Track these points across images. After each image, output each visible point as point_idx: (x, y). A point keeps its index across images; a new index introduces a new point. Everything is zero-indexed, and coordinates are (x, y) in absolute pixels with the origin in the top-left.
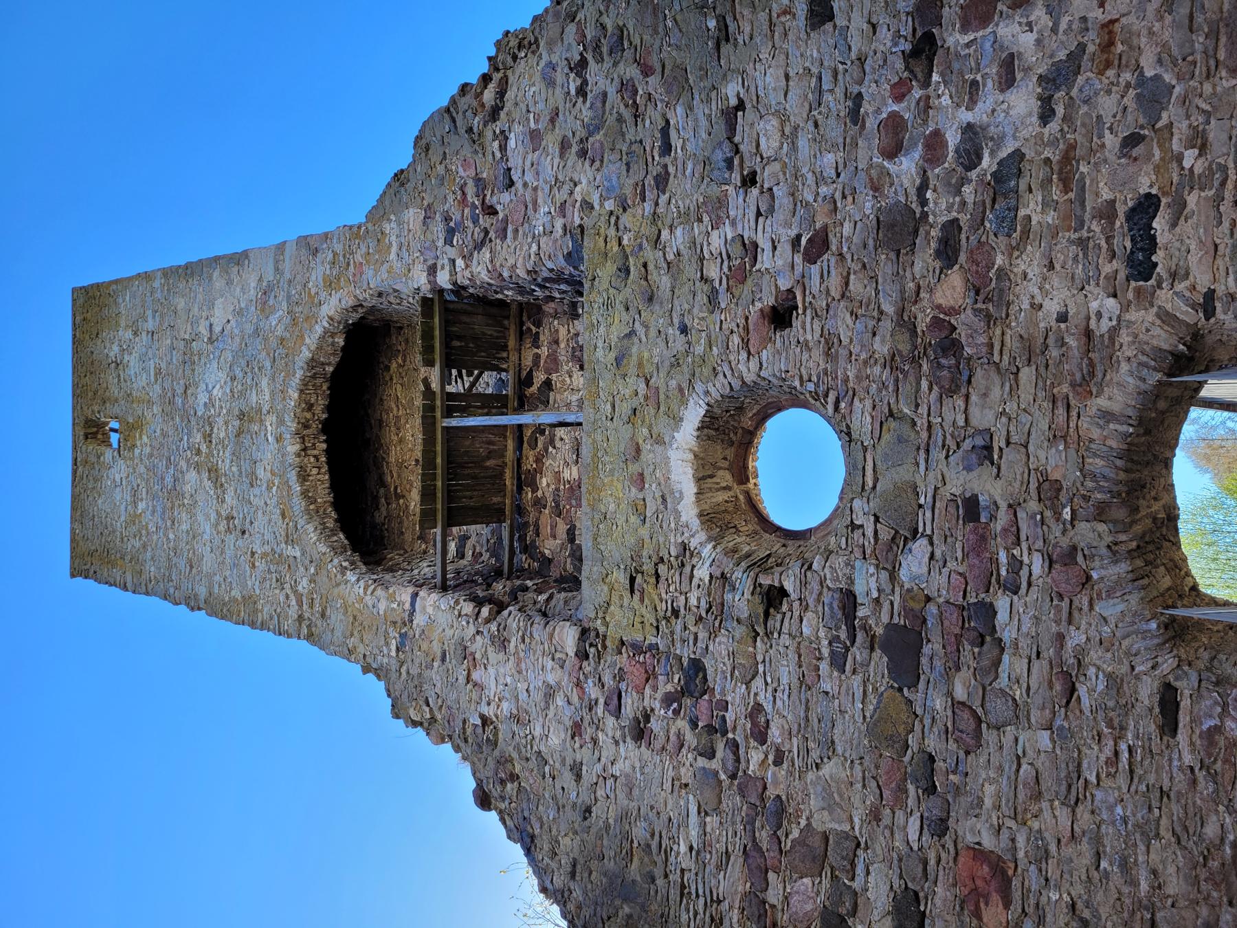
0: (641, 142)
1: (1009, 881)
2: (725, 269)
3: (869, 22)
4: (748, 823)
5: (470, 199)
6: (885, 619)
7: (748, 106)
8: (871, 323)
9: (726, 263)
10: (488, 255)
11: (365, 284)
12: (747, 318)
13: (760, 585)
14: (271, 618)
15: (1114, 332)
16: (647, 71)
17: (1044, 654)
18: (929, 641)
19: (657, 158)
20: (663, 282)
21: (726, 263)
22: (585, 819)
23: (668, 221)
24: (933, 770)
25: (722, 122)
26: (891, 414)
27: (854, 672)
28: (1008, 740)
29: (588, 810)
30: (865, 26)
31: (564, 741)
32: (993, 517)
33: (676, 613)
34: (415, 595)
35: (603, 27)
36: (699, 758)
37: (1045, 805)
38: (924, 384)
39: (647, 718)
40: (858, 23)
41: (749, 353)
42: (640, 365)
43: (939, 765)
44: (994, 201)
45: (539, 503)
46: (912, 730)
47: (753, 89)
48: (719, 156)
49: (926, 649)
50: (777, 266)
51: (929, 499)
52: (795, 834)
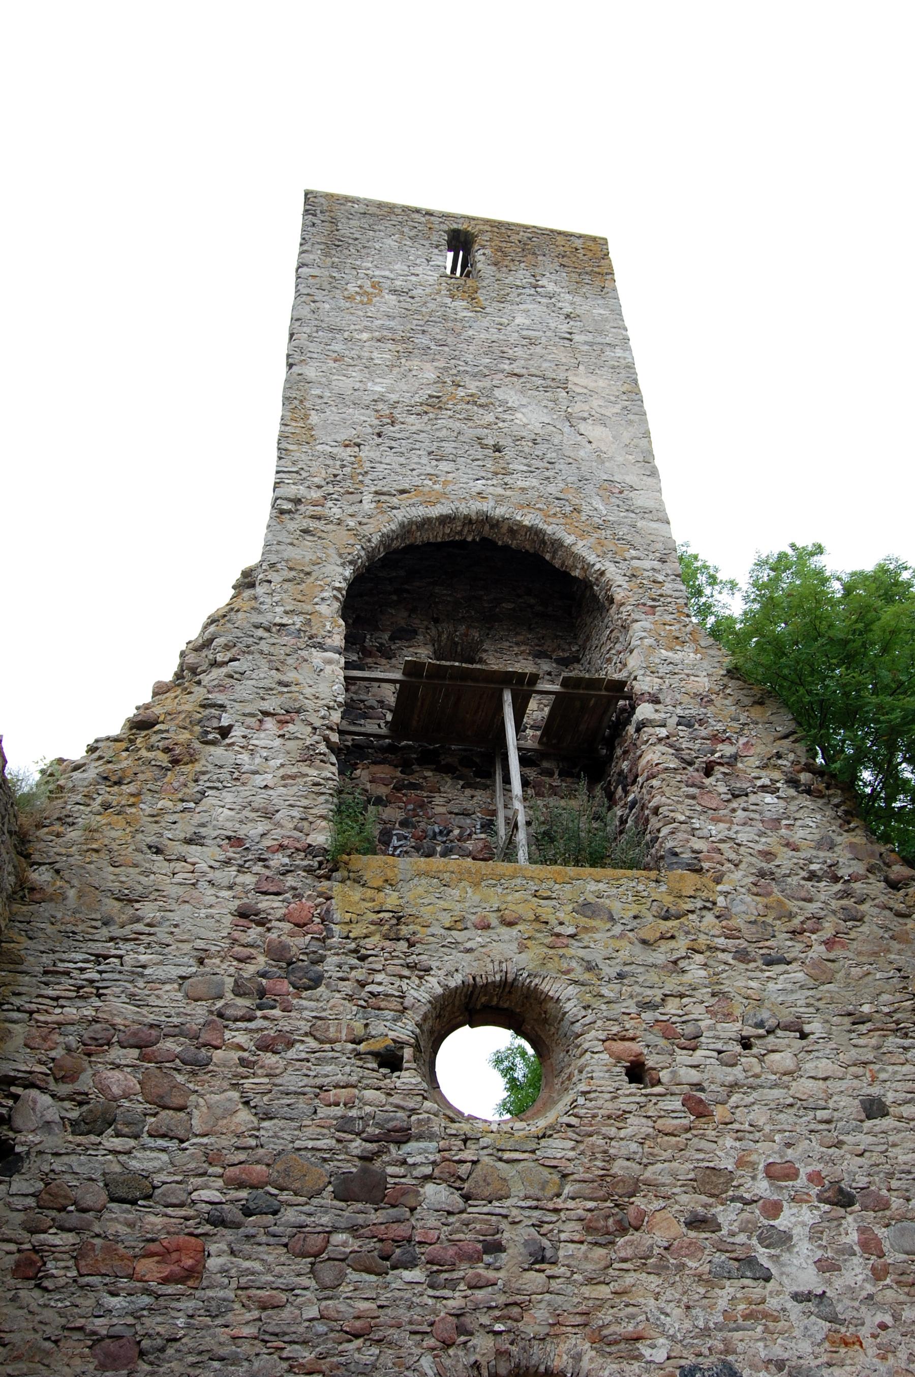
0: (774, 936)
1: (183, 1283)
2: (674, 1019)
3: (865, 1151)
4: (181, 1030)
5: (720, 747)
6: (390, 1170)
7: (804, 1042)
8: (637, 1157)
9: (679, 1019)
10: (672, 766)
11: (637, 617)
12: (633, 1039)
13: (402, 1048)
14: (294, 463)
15: (638, 1357)
16: (829, 944)
17: (381, 1312)
18: (376, 1210)
19: (762, 952)
20: (660, 956)
21: (679, 1019)
22: (150, 847)
23: (711, 962)
24: (266, 1214)
25: (790, 1018)
26: (565, 1176)
27: (339, 1141)
28: (305, 1281)
29: (159, 851)
30: (862, 1147)
32: (488, 1266)
33: (363, 958)
35: (862, 902)
36: (232, 979)
37: (256, 1314)
38: (591, 1204)
39: (261, 924)
40: (866, 1140)
41: (604, 1041)
42: (586, 929)
44: (736, 1259)
46: (296, 1194)
47: (816, 1048)
48: (765, 1015)
50: (680, 1068)
51: (498, 1211)
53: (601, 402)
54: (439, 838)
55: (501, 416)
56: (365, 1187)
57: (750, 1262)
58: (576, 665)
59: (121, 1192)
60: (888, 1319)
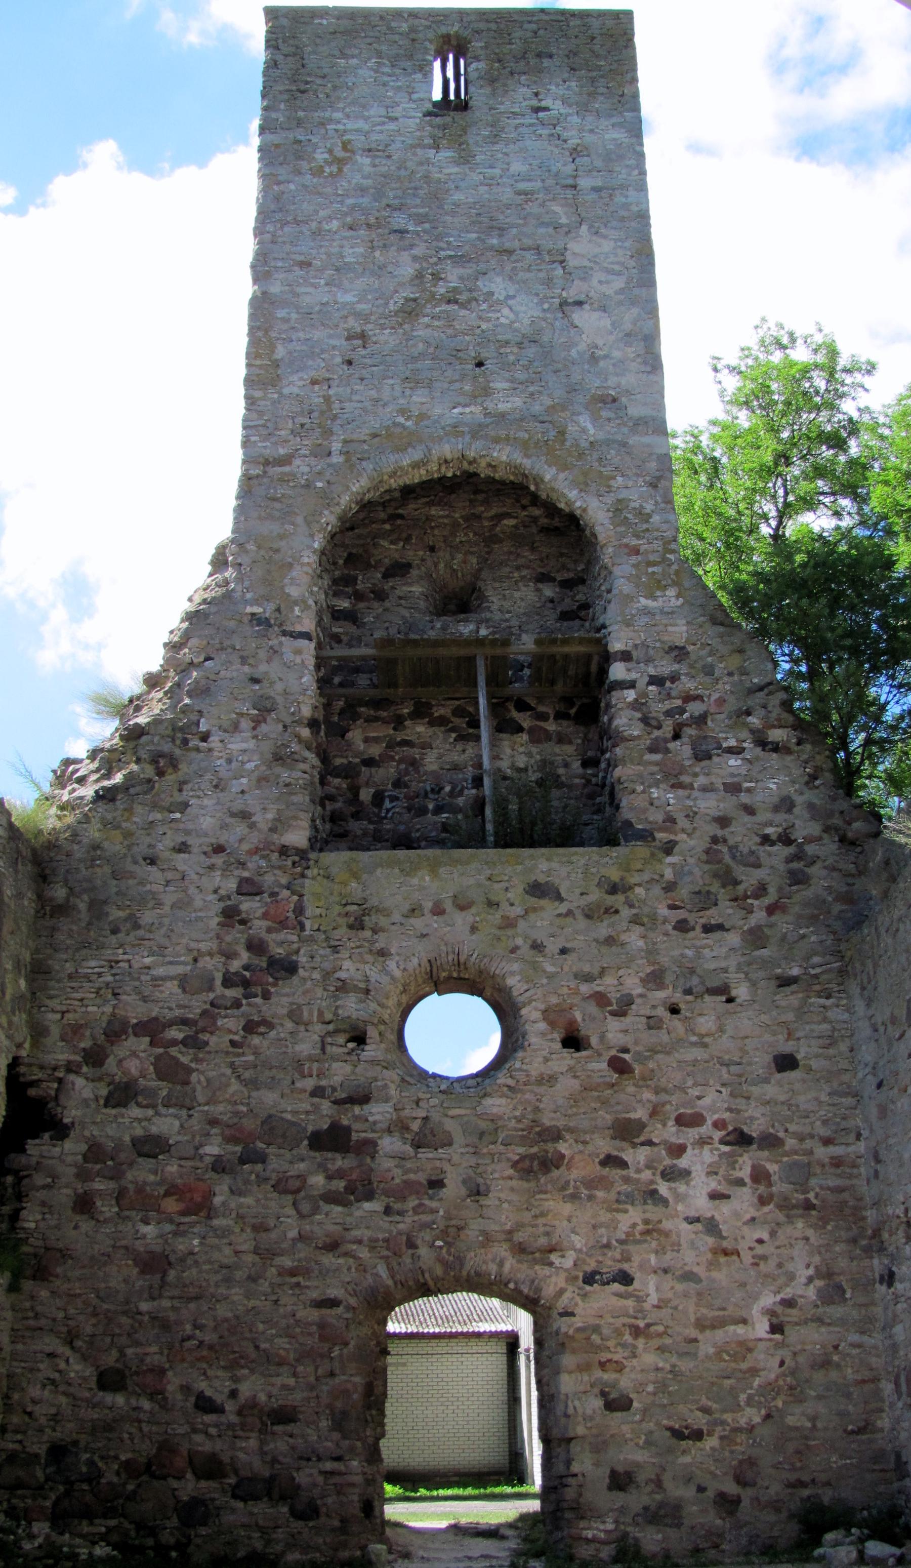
15: (551, 1264)
22: (145, 859)
31: (206, 835)
34: (306, 636)
43: (259, 1167)
45: (398, 722)
48: (695, 981)
49: (338, 1156)
52: (184, 1059)
53: (603, 277)
54: (431, 796)
55: (484, 315)
56: (333, 1139)
57: (653, 1195)
58: (580, 587)
59: (146, 1149)
60: (765, 1236)
